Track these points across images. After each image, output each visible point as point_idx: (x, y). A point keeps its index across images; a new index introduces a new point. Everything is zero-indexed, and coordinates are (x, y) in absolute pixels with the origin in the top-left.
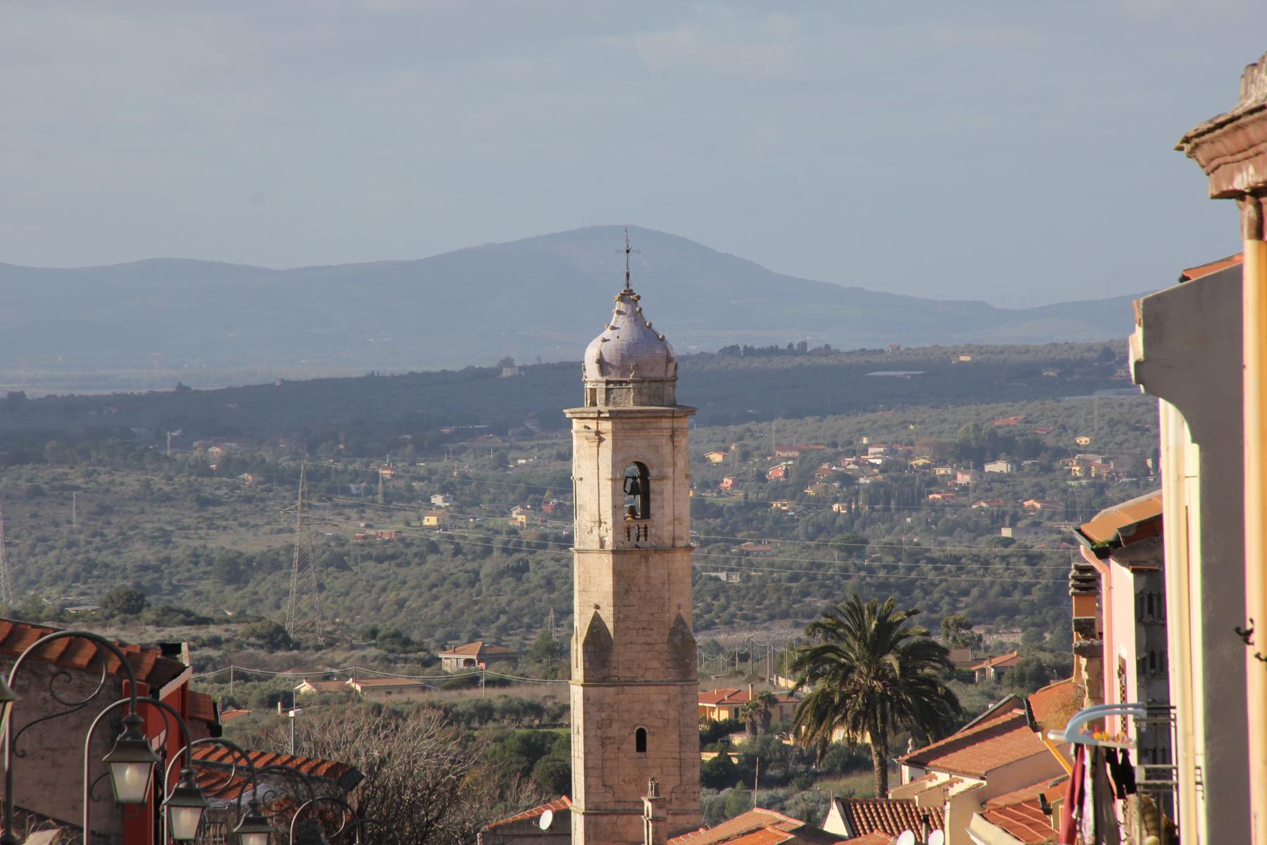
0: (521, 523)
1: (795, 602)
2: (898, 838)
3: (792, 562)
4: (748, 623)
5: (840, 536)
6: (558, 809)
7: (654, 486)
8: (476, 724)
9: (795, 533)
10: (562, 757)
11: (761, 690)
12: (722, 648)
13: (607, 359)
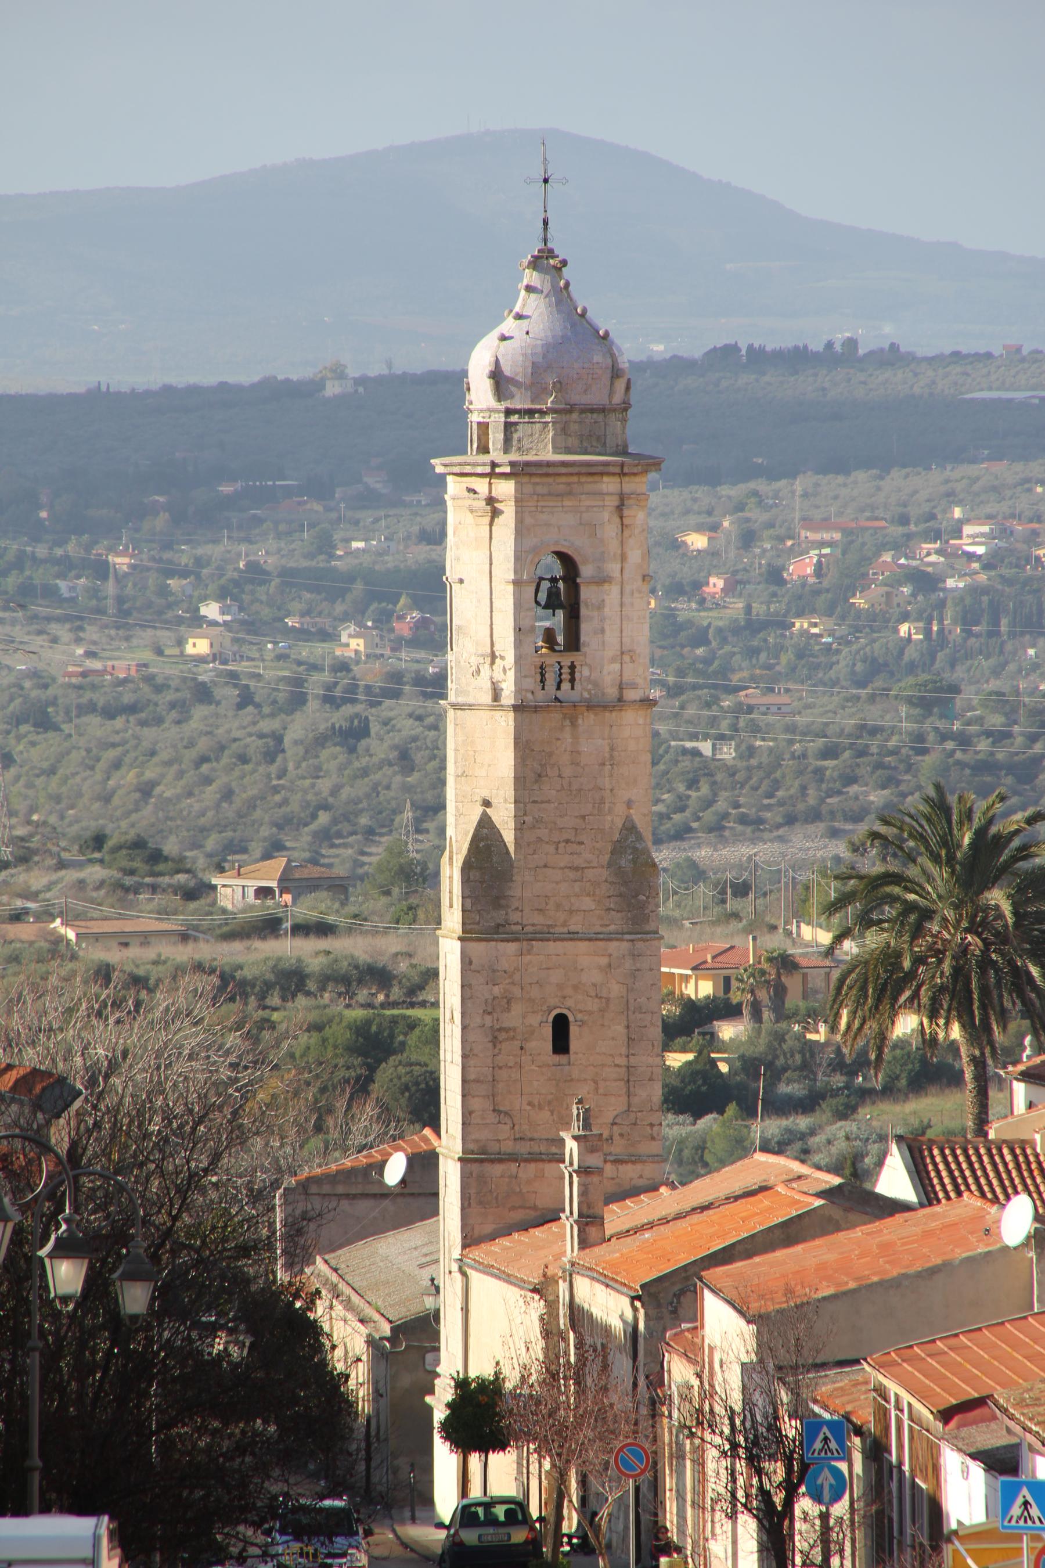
0: (356, 652)
1: (831, 793)
2: (1004, 1206)
3: (826, 724)
4: (749, 830)
5: (911, 680)
6: (415, 1151)
7: (586, 593)
8: (275, 1000)
9: (832, 673)
10: (423, 1059)
11: (770, 946)
12: (704, 872)
13: (507, 370)
